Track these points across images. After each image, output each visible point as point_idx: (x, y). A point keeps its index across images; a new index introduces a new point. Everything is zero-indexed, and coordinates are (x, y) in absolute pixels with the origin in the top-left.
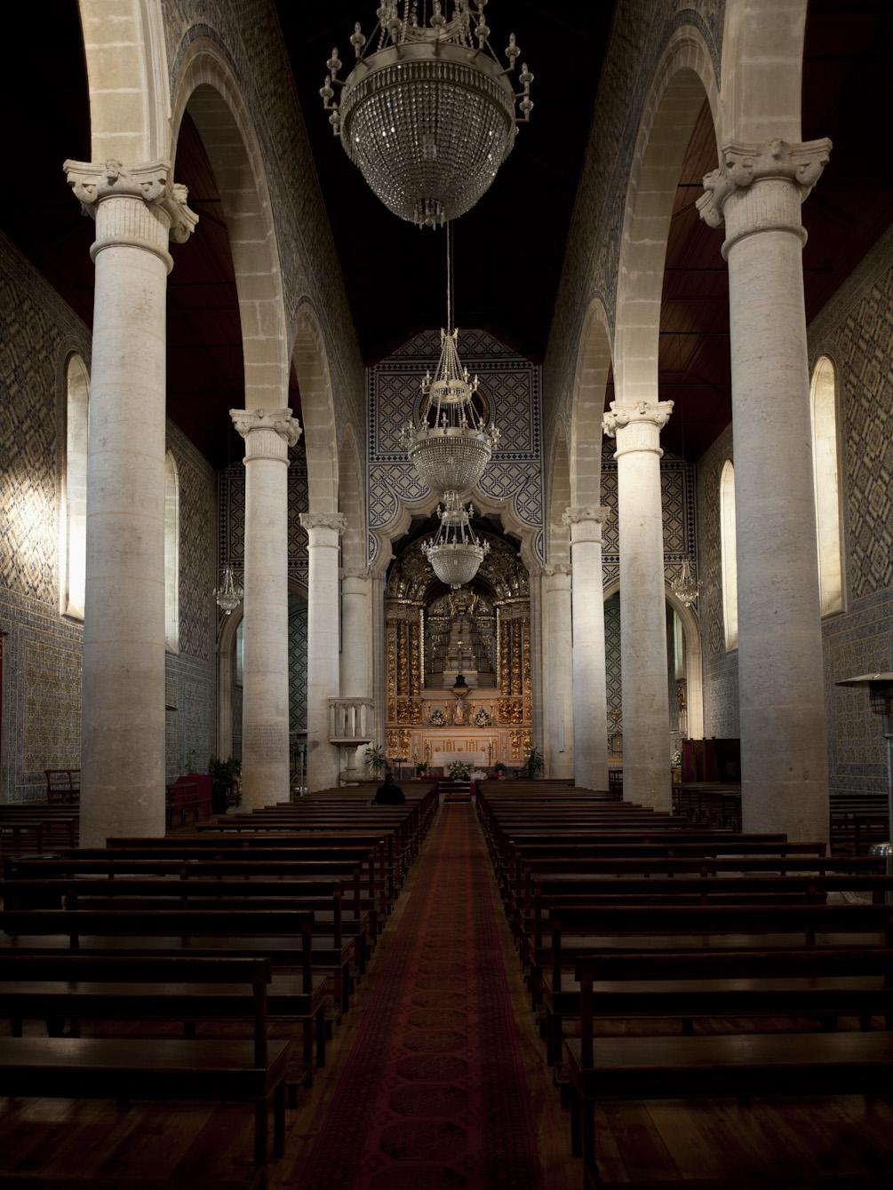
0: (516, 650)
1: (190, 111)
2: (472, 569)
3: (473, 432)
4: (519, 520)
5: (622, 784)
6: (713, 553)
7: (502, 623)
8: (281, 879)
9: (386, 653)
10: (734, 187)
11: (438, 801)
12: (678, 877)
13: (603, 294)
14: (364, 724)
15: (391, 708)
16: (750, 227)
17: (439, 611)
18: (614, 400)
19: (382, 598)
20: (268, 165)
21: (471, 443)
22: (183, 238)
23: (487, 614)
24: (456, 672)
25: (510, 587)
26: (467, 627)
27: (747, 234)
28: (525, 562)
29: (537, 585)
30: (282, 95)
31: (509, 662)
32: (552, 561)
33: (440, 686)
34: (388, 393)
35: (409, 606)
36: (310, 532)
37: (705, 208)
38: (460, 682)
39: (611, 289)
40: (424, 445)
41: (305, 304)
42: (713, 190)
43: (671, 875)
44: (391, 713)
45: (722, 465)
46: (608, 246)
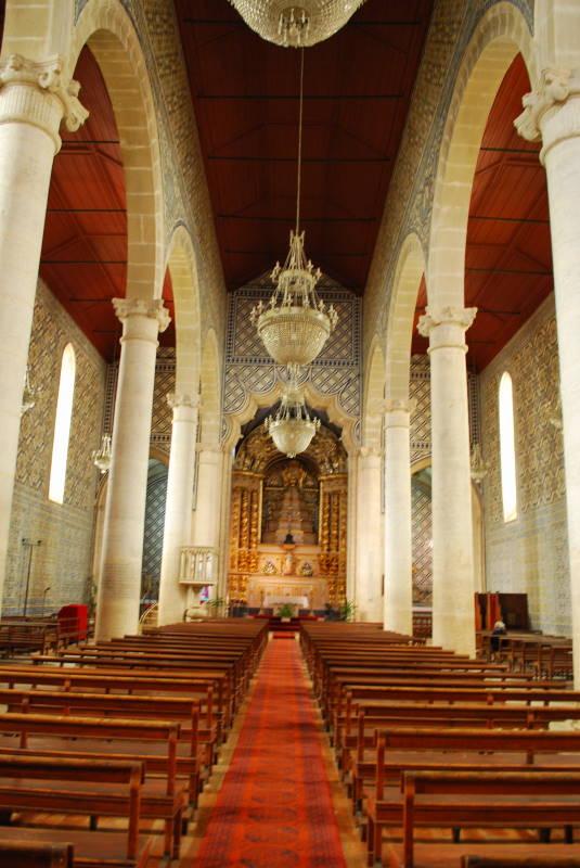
0: (334, 515)
1: (94, 50)
2: (304, 444)
3: (313, 312)
4: (342, 413)
5: (431, 618)
6: (493, 444)
7: (325, 494)
8: (107, 693)
9: (232, 513)
10: (551, 101)
11: (267, 638)
12: (458, 705)
13: (418, 229)
14: (207, 570)
15: (233, 559)
16: (566, 133)
17: (275, 483)
18: (528, 90)
19: (230, 468)
20: (159, 114)
21: (315, 322)
22: (73, 127)
23: (312, 487)
24: (287, 532)
25: (331, 466)
26: (296, 495)
27: (564, 138)
28: (345, 445)
29: (354, 463)
30: (175, 72)
31: (329, 525)
32: (367, 445)
33: (273, 542)
34: (243, 336)
35: (251, 477)
36: (175, 410)
37: (523, 125)
38: (289, 539)
39: (426, 221)
40: (273, 321)
41: (181, 227)
42: (531, 107)
43: (546, 704)
44: (233, 562)
45: (501, 375)
46: (423, 192)
